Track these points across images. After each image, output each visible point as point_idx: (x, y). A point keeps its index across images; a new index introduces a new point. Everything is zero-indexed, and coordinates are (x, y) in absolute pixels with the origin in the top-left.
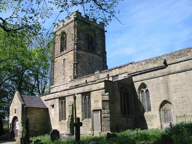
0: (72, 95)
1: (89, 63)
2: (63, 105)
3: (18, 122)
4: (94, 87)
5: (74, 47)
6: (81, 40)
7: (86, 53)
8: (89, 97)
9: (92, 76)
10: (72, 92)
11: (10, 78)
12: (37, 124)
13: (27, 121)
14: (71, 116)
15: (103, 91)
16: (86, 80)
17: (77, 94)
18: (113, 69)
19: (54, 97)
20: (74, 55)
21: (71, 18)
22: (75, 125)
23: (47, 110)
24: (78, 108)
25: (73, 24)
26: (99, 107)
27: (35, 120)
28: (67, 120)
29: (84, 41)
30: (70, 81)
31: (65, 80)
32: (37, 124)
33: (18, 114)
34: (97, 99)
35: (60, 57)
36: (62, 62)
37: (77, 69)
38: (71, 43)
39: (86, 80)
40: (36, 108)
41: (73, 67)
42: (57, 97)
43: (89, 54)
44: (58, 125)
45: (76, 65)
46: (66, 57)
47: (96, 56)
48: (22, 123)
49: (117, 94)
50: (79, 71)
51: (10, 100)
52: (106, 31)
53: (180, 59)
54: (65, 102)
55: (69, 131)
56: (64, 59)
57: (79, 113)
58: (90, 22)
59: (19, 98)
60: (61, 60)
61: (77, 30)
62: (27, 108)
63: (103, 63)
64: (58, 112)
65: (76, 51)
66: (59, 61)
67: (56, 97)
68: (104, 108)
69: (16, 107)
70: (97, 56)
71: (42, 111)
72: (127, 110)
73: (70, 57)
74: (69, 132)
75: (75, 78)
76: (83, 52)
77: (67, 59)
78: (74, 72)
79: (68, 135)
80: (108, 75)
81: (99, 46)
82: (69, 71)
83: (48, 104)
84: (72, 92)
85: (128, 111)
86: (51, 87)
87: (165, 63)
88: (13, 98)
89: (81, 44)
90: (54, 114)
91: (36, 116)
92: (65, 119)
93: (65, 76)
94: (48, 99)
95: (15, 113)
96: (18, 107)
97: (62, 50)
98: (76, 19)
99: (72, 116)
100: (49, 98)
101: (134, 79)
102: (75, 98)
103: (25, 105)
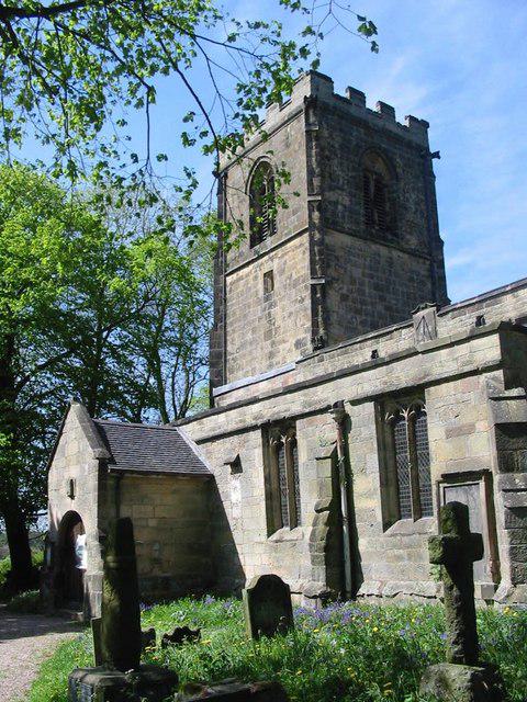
0: (329, 407)
1: (377, 287)
2: (284, 460)
3: (84, 536)
4: (444, 363)
5: (310, 216)
6: (339, 189)
7: (359, 243)
8: (419, 413)
9: (404, 331)
10: (326, 394)
11: (51, 365)
12: (165, 545)
14: (326, 509)
15: (494, 379)
16: (375, 352)
17: (354, 403)
18: (507, 293)
19: (241, 426)
20: (312, 251)
21: (288, 103)
23: (208, 484)
24: (363, 471)
25: (299, 126)
26: (476, 461)
27: (158, 529)
28: (306, 529)
29: (351, 195)
30: (300, 358)
31: (274, 360)
32: (165, 545)
33: (84, 502)
34: (465, 420)
35: (251, 267)
36: (261, 286)
37: (326, 311)
38: (295, 210)
39: (375, 352)
40: (158, 473)
41: (308, 302)
42: (254, 422)
43: (374, 247)
44: (260, 549)
45: (319, 296)
46: (275, 265)
47: (401, 254)
48: (102, 539)
50: (334, 318)
51: (46, 451)
52: (437, 155)
54: (294, 444)
55: (323, 576)
56: (269, 275)
57: (369, 495)
58: (369, 116)
59: (84, 429)
60: (256, 277)
61: (321, 149)
62: (122, 473)
63: (429, 286)
65: (317, 236)
66: (245, 284)
67: (250, 421)
69: (74, 473)
70: (406, 256)
73: (293, 260)
74: (320, 586)
75: (321, 344)
76: (346, 240)
77: (282, 272)
78: (315, 324)
79: (315, 597)
81: (410, 216)
82: (290, 322)
83: (212, 460)
84: (326, 394)
86: (216, 391)
88: (61, 434)
89: (340, 207)
90: (243, 500)
91: (160, 512)
92: (295, 523)
93: (273, 343)
94: (211, 434)
95: (72, 497)
96: (83, 469)
97: (256, 239)
98: (310, 102)
99: (334, 506)
100: (217, 432)
102: (344, 424)
103: (112, 461)
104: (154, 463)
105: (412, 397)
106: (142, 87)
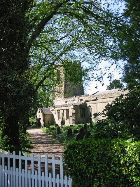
10: (62, 108)
13: (44, 119)
22: (63, 123)
49: (79, 110)
53: (101, 98)
64: (57, 116)
65: (65, 83)
68: (73, 116)
71: (50, 115)
72: (83, 116)
80: (79, 99)
83: (53, 112)
84: (62, 108)
85: (84, 115)
87: (97, 98)
90: (56, 116)
101: (87, 103)
102: (64, 111)
104: (47, 113)
105: (68, 110)
106: (52, 25)
